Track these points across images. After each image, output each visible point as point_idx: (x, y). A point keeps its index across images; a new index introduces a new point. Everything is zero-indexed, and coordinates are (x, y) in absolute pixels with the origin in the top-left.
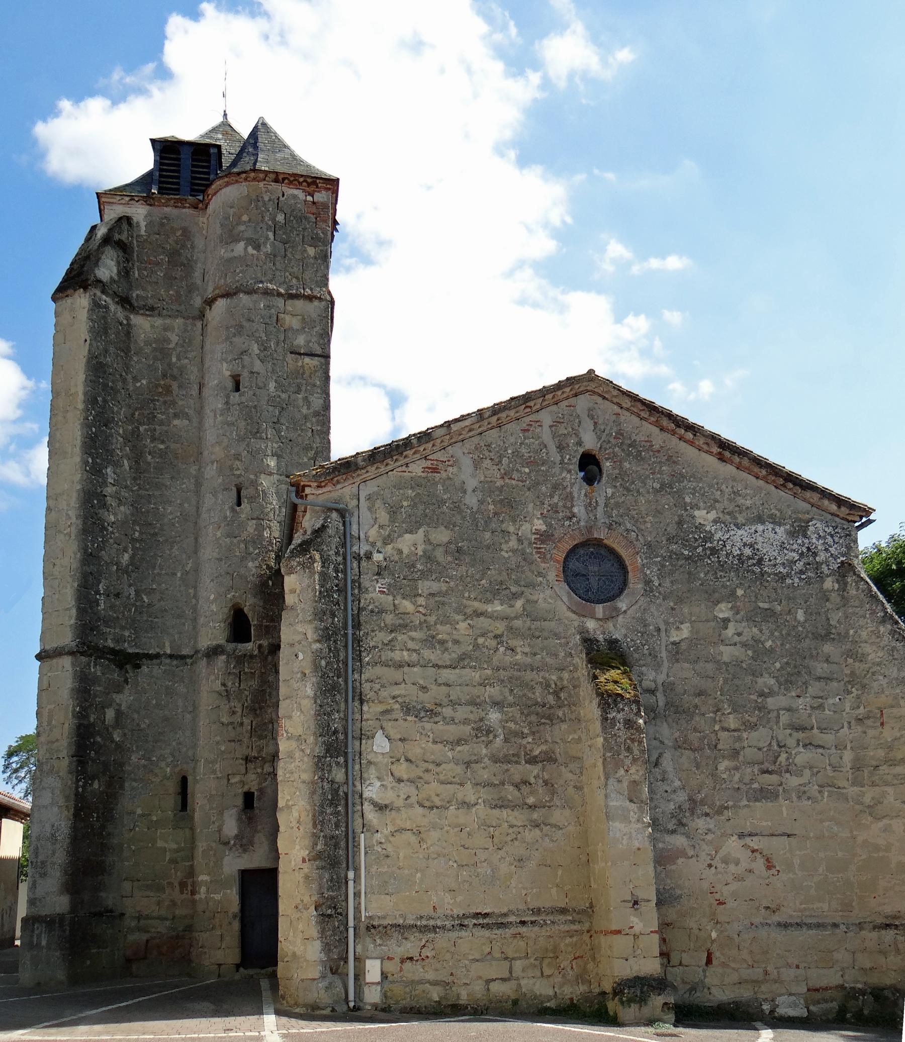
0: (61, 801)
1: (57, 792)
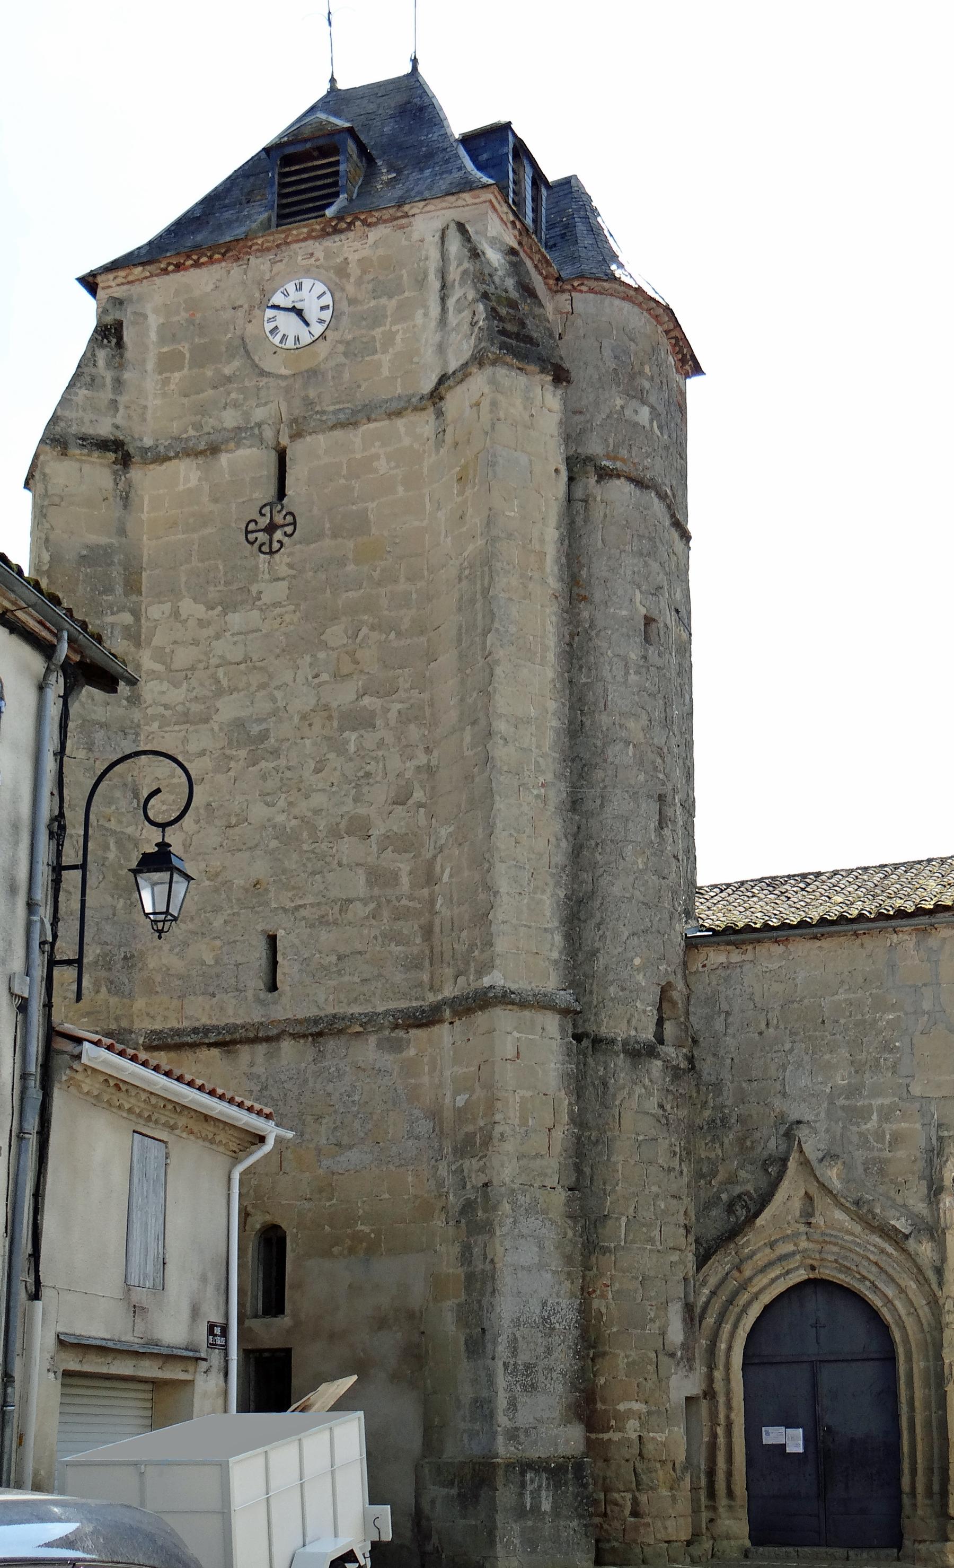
0: (556, 1263)
1: (549, 1246)
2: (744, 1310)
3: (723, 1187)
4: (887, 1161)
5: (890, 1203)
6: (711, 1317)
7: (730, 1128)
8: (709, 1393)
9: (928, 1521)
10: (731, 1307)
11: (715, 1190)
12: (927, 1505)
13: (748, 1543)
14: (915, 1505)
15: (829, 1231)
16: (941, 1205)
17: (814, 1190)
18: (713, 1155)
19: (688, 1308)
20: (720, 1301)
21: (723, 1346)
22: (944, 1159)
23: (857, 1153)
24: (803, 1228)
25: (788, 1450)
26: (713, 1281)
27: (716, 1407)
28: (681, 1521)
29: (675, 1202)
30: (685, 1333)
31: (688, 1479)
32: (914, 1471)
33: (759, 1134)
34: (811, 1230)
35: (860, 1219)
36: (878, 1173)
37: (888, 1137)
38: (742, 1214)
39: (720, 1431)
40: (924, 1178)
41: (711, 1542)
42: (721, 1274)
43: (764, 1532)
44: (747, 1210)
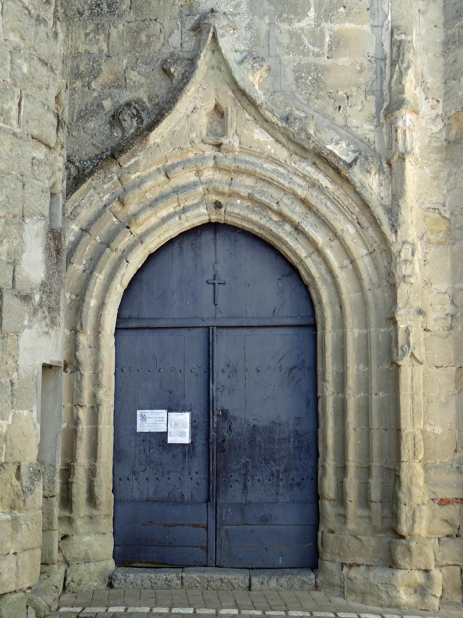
2: (124, 257)
3: (107, 91)
4: (325, 69)
5: (327, 122)
6: (80, 263)
7: (120, 16)
8: (72, 364)
9: (362, 537)
10: (108, 250)
11: (95, 94)
12: (361, 517)
13: (111, 564)
14: (344, 517)
15: (244, 157)
16: (400, 123)
17: (228, 100)
18: (94, 50)
19: (55, 236)
20: (93, 242)
21: (93, 302)
22: (405, 65)
23: (286, 57)
24: (210, 152)
25: (170, 440)
26: (85, 214)
27: (79, 383)
28: (25, 557)
29: (44, 71)
30: (48, 269)
31: (39, 491)
32: (342, 469)
33: (158, 26)
34: (220, 155)
35: (289, 139)
36: (313, 84)
37: (327, 39)
38: (131, 126)
39: (83, 414)
40: (373, 93)
41: (63, 568)
42: (97, 205)
43: (132, 551)
44: (136, 123)
